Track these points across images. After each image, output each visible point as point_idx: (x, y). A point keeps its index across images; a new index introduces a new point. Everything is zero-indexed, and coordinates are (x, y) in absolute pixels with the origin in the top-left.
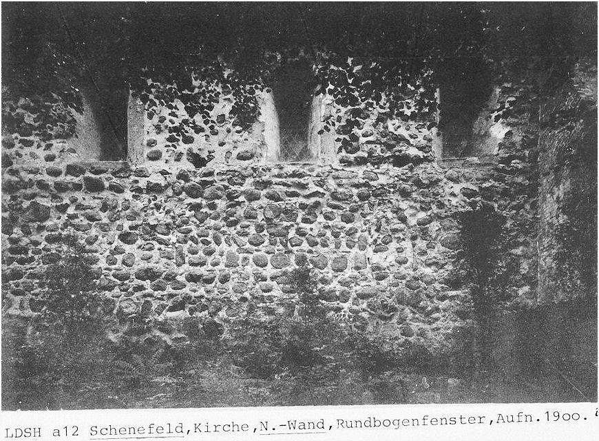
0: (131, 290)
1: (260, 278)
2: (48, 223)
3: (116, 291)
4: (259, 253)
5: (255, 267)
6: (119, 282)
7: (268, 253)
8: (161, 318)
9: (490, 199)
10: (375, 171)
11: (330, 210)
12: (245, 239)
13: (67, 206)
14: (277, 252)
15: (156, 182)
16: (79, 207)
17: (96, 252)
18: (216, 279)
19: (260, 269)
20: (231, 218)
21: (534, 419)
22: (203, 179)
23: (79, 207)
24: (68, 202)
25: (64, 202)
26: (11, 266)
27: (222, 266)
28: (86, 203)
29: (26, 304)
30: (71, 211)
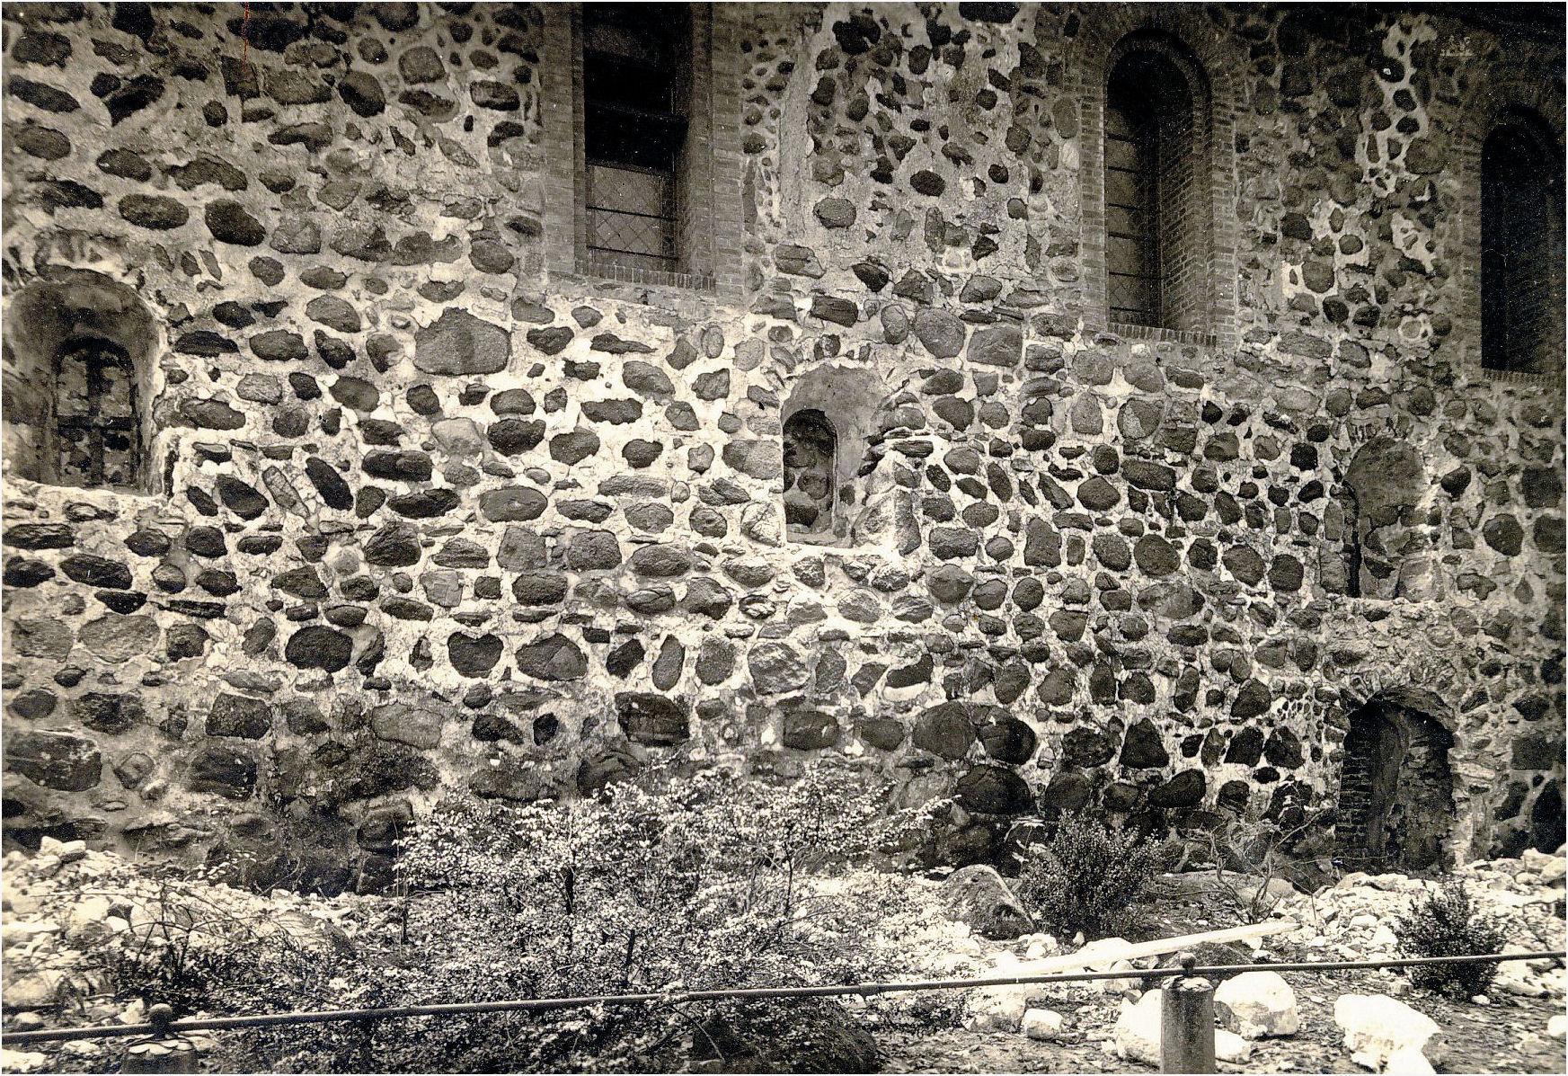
0: (780, 617)
1: (1115, 599)
2: (497, 383)
3: (733, 619)
4: (1106, 530)
5: (1100, 568)
6: (740, 592)
7: (1128, 531)
8: (869, 706)
9: (1289, 518)
10: (1363, 342)
11: (1268, 431)
12: (1072, 488)
13: (567, 335)
14: (1147, 531)
15: (844, 296)
16: (605, 343)
17: (659, 492)
18: (1008, 599)
19: (1116, 575)
20: (1038, 427)
21: (1396, 1045)
22: (972, 306)
23: (605, 343)
24: (572, 323)
25: (557, 323)
26: (375, 519)
27: (1017, 561)
28: (627, 333)
29: (439, 650)
30: (580, 350)
